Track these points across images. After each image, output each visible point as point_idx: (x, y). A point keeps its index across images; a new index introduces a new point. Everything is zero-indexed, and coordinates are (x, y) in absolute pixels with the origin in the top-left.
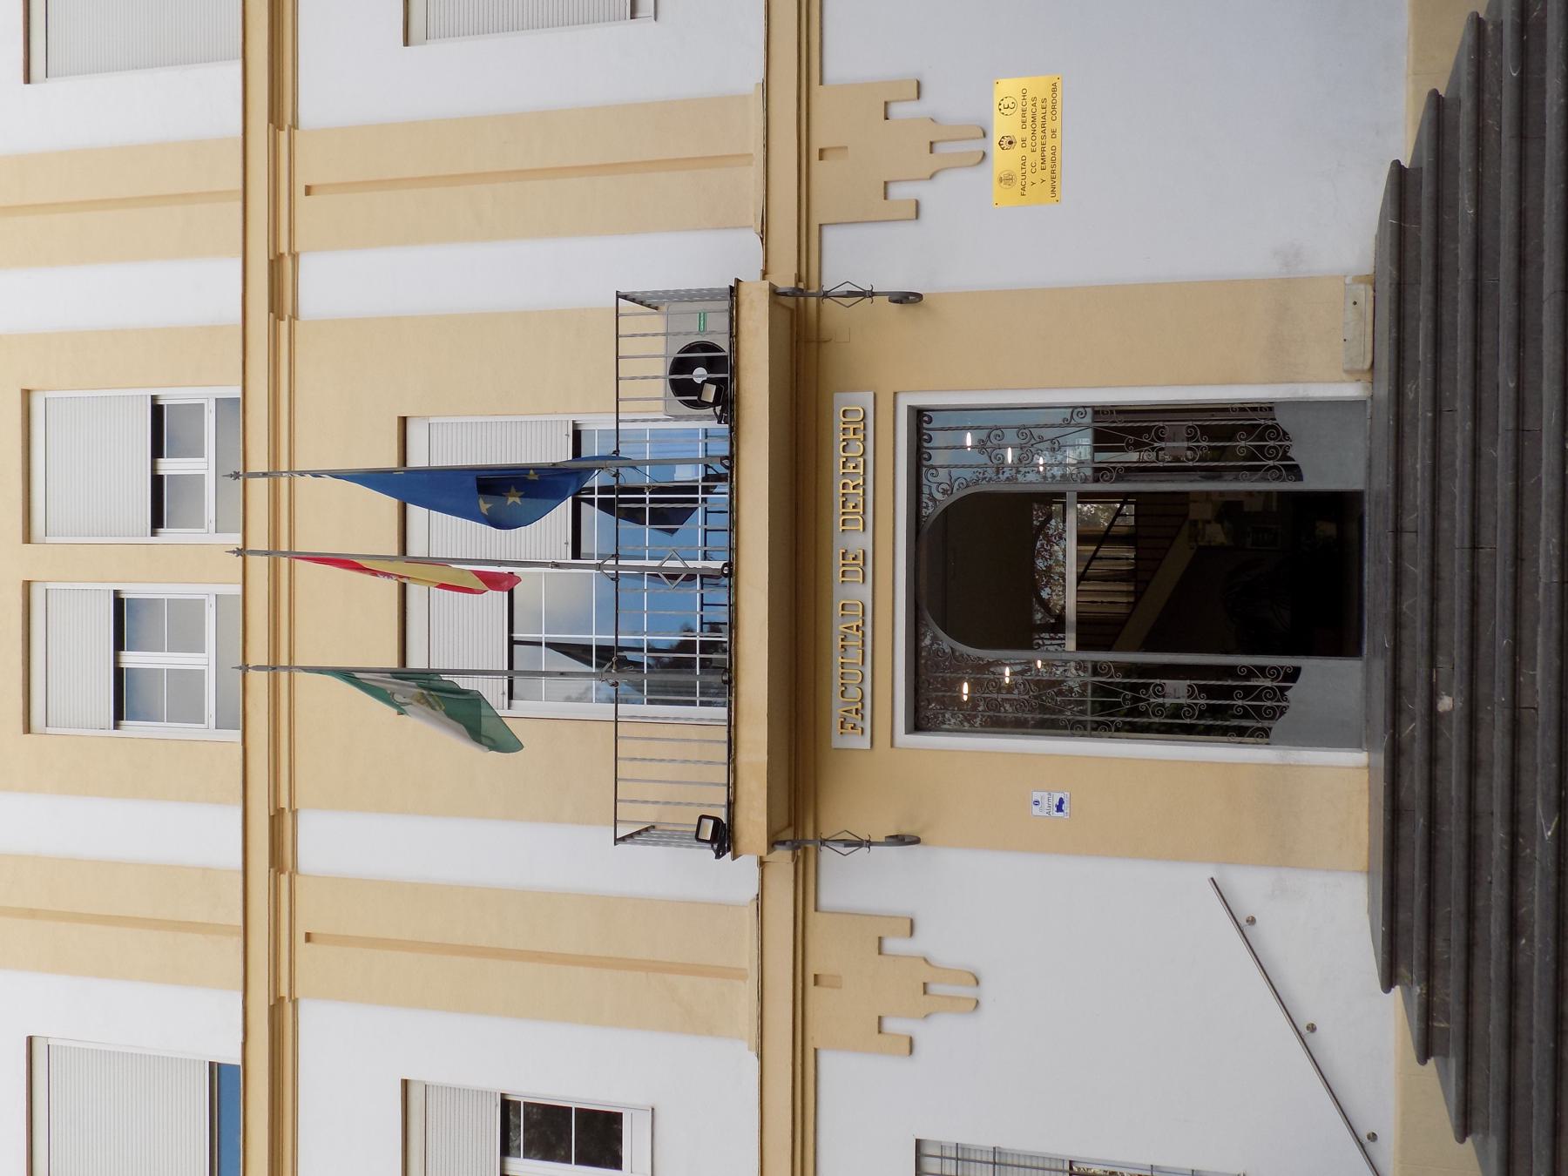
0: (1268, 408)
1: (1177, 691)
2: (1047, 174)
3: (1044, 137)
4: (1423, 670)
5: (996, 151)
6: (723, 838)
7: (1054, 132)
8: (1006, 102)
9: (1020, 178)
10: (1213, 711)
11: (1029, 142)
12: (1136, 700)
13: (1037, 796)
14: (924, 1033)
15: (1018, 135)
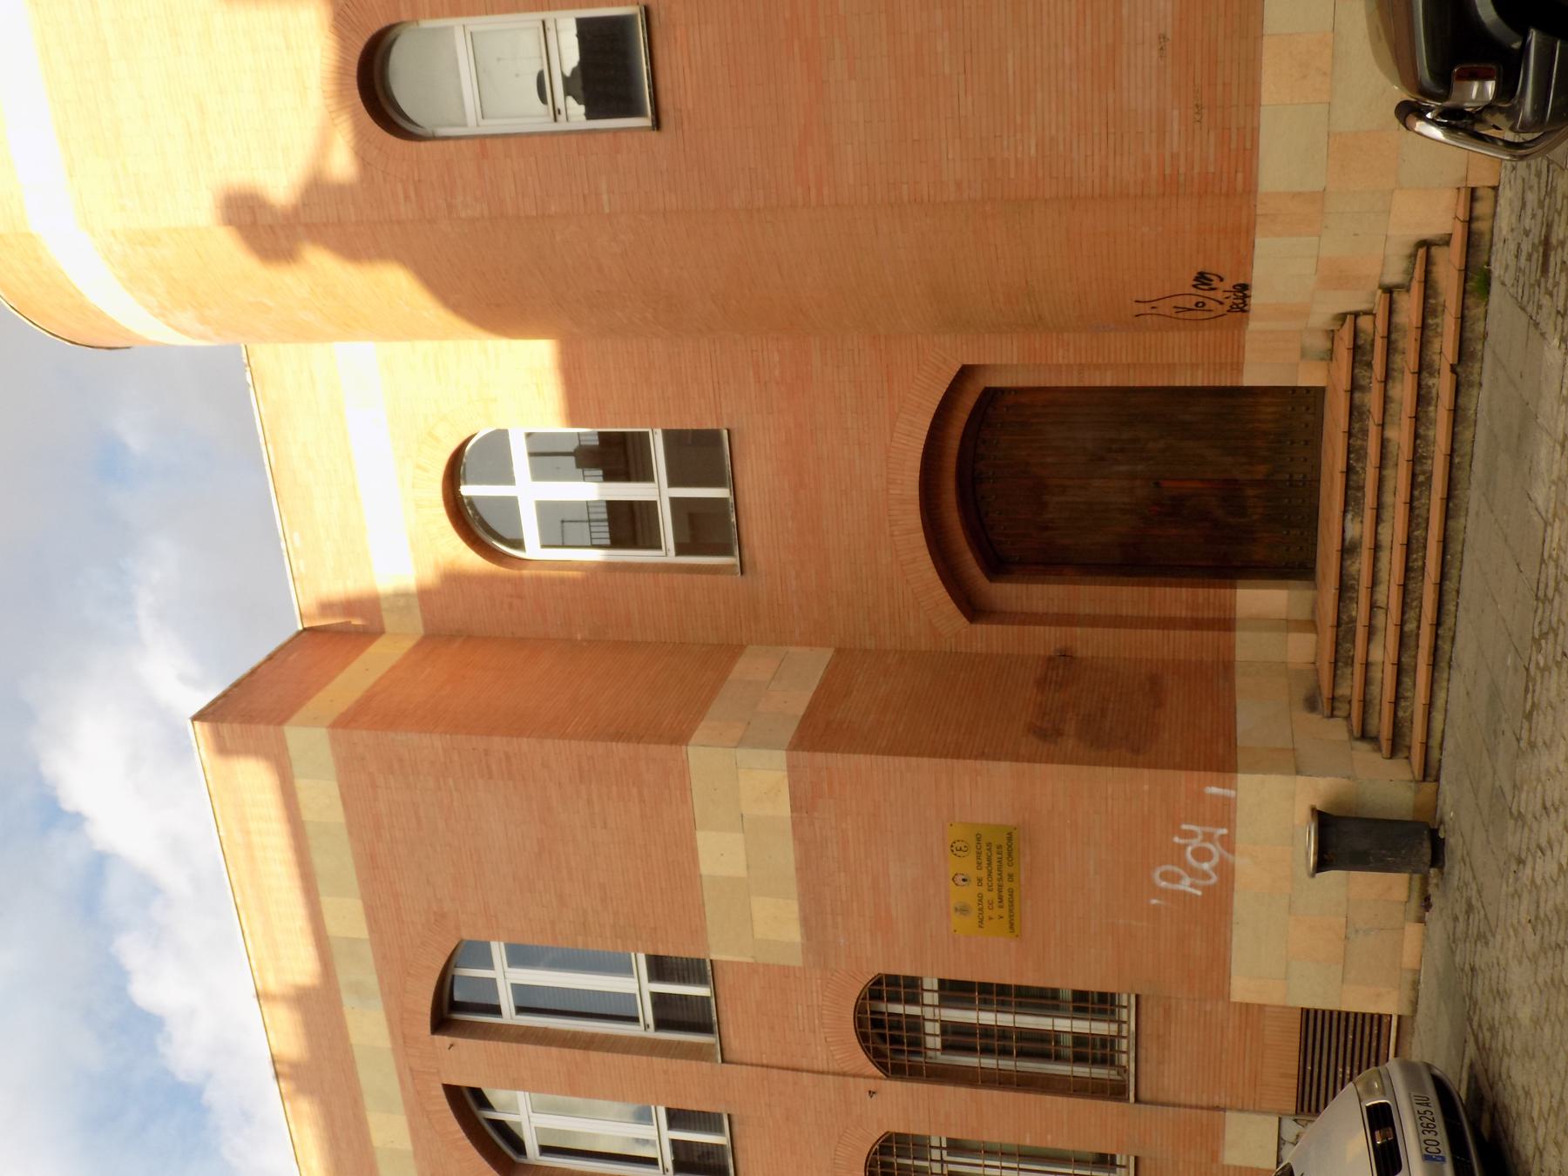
2: (1005, 912)
3: (1000, 879)
7: (1153, 308)
8: (958, 845)
11: (985, 882)
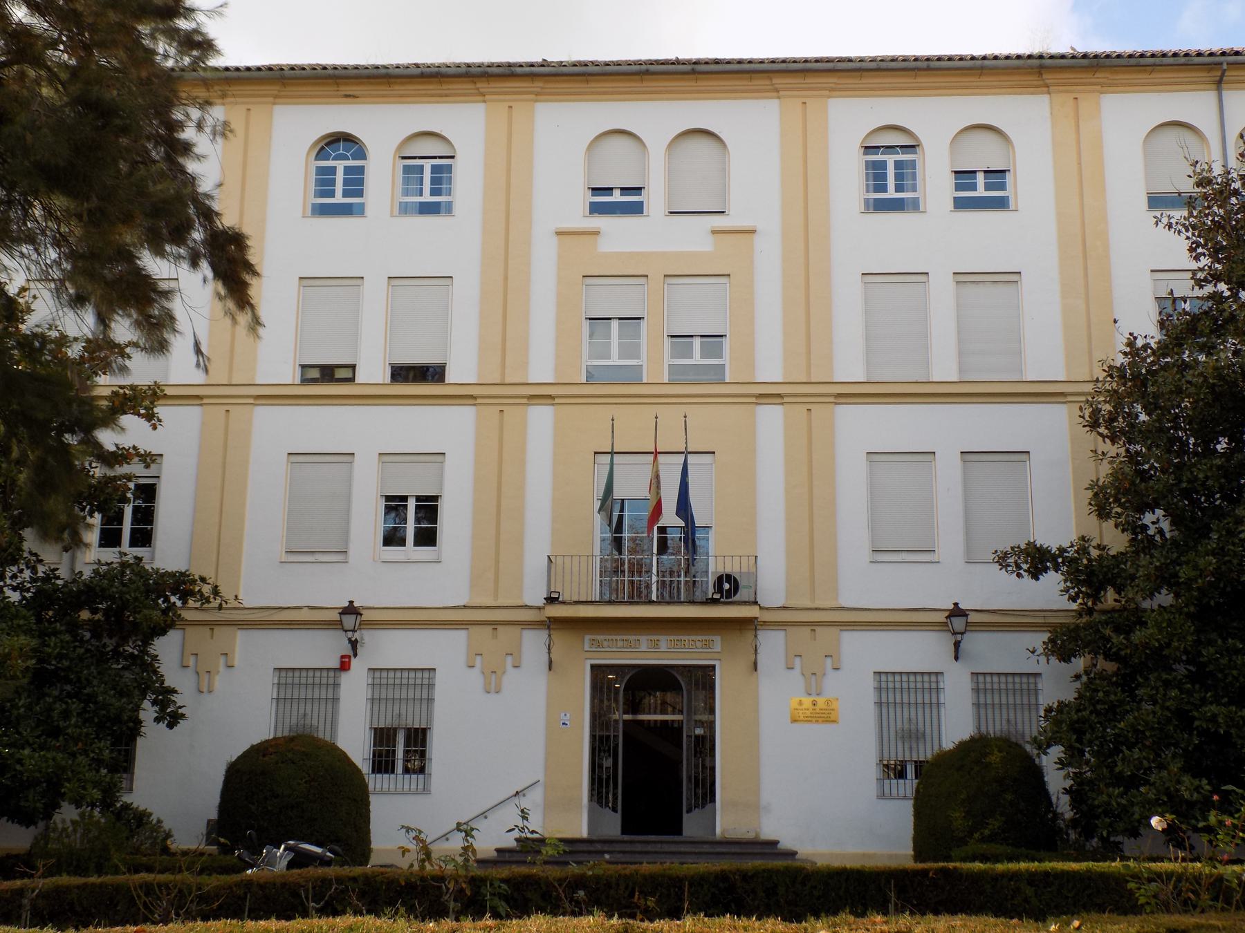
0: (713, 800)
1: (608, 763)
4: (618, 849)
5: (811, 699)
6: (551, 600)
9: (801, 708)
10: (600, 779)
12: (604, 751)
13: (568, 715)
14: (476, 671)
15: (817, 707)
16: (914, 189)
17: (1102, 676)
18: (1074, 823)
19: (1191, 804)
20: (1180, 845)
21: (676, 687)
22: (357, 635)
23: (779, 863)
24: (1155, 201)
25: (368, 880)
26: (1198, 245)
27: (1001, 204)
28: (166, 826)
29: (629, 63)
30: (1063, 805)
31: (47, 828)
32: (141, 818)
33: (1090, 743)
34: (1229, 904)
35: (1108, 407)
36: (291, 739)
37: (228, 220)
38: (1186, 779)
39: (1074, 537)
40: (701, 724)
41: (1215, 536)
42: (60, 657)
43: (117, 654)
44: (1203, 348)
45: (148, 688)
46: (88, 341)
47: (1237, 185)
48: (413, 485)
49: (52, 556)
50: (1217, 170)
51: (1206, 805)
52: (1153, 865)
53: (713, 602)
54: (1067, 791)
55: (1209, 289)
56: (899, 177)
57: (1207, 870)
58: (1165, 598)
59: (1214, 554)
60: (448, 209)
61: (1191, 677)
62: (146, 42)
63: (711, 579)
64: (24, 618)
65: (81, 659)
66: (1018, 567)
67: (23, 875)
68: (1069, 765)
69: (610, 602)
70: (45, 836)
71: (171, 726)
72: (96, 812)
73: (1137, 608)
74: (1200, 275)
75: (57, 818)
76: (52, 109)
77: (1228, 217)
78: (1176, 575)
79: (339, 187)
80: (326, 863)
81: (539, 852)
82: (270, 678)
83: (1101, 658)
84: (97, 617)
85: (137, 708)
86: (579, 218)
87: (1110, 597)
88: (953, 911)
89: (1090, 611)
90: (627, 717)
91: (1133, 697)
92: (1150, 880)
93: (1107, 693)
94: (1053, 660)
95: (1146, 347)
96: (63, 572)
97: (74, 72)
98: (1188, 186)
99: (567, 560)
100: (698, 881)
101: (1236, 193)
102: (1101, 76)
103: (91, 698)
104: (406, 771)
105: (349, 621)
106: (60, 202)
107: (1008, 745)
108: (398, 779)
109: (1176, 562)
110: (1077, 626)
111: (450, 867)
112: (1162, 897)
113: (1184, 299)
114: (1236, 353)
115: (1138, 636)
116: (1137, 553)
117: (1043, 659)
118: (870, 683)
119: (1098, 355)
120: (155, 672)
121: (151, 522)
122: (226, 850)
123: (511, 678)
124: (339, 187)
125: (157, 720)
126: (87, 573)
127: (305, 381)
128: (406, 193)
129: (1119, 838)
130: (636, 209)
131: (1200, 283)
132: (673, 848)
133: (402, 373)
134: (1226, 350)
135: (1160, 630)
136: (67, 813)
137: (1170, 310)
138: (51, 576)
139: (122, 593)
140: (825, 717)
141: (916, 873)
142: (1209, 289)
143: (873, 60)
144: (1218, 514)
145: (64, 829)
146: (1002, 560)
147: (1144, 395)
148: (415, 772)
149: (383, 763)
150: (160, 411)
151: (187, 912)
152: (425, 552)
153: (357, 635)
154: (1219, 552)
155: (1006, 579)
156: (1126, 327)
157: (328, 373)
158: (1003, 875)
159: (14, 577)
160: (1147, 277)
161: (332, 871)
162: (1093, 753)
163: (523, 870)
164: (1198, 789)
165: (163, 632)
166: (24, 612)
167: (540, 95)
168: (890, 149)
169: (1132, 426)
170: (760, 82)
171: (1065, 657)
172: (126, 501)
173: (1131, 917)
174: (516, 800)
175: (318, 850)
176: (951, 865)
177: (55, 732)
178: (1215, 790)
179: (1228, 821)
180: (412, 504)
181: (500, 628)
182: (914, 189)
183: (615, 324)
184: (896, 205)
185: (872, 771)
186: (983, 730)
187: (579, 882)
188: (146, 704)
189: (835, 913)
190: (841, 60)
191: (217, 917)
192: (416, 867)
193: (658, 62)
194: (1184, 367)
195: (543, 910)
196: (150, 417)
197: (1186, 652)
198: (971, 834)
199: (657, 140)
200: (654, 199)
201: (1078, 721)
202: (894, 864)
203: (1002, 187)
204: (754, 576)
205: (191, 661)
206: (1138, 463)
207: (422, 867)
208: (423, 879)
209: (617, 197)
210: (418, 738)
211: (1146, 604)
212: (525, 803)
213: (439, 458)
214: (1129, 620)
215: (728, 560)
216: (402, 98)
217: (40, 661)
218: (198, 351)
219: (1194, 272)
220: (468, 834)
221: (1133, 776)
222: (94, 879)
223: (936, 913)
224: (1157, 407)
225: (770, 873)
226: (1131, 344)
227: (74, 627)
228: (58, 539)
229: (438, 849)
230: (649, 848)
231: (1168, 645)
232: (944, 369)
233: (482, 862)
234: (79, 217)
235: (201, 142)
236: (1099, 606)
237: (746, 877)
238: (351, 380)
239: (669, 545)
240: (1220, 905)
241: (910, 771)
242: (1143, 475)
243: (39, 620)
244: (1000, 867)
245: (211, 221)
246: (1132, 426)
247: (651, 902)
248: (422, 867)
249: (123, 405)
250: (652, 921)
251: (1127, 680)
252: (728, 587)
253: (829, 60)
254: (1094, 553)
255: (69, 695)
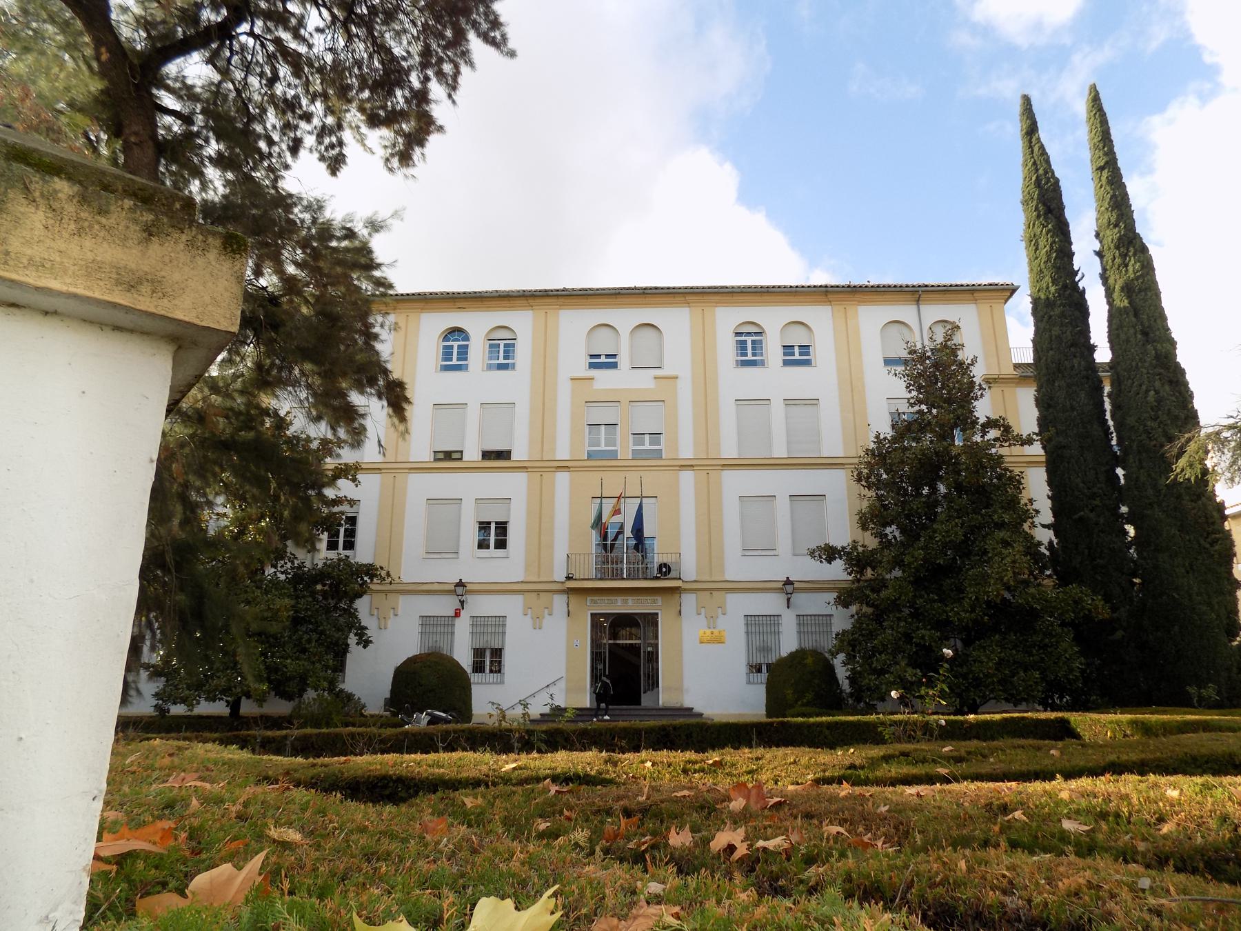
1: (600, 667)
6: (569, 578)
14: (528, 618)
16: (762, 355)
17: (865, 615)
18: (851, 695)
19: (912, 683)
20: (906, 705)
21: (637, 625)
22: (464, 598)
23: (693, 721)
24: (888, 362)
25: (471, 731)
26: (910, 385)
27: (807, 363)
28: (363, 701)
29: (609, 289)
30: (845, 685)
31: (300, 702)
32: (350, 697)
33: (859, 652)
34: (932, 736)
35: (866, 471)
36: (429, 654)
37: (396, 375)
38: (910, 670)
39: (850, 541)
40: (650, 645)
41: (922, 539)
42: (307, 610)
43: (336, 608)
44: (914, 439)
45: (352, 626)
46: (321, 439)
47: (929, 354)
48: (493, 516)
49: (302, 555)
50: (919, 346)
51: (920, 684)
52: (891, 717)
53: (656, 578)
54: (847, 678)
55: (916, 408)
56: (753, 348)
57: (920, 718)
58: (897, 573)
59: (922, 549)
60: (513, 366)
61: (911, 615)
62: (356, 282)
63: (656, 566)
64: (288, 589)
65: (317, 610)
66: (821, 557)
67: (287, 728)
68: (848, 664)
69: (601, 579)
70: (299, 707)
71: (365, 647)
72: (326, 693)
73: (883, 579)
74: (912, 401)
75: (305, 696)
76: (306, 318)
77: (925, 371)
78: (903, 561)
79: (455, 356)
80: (448, 722)
81: (563, 716)
82: (417, 622)
83: (864, 606)
84: (326, 588)
85: (347, 637)
86: (582, 370)
87: (869, 573)
88: (786, 745)
89: (858, 581)
90: (610, 642)
91: (881, 625)
92: (890, 725)
93: (867, 625)
94: (840, 607)
95: (885, 439)
96: (308, 564)
97: (318, 299)
98: (904, 354)
99: (578, 556)
100: (650, 731)
101: (929, 358)
102: (858, 297)
103: (322, 633)
104: (491, 671)
105: (459, 590)
106: (308, 367)
107: (816, 653)
108: (487, 676)
109: (903, 554)
110: (852, 589)
111: (516, 724)
112: (896, 734)
113: (904, 414)
114: (931, 442)
115: (883, 594)
116: (882, 549)
117: (834, 607)
118: (742, 621)
119: (861, 443)
120: (356, 618)
121: (354, 537)
122: (395, 715)
123: (547, 621)
124: (455, 356)
125: (358, 644)
126: (320, 565)
127: (436, 460)
128: (490, 358)
129: (875, 702)
130: (614, 366)
131: (912, 405)
132: (637, 713)
133: (487, 455)
134: (926, 440)
135: (895, 591)
136: (311, 694)
137: (897, 419)
138: (301, 566)
139: (338, 575)
140: (719, 640)
141: (767, 724)
142: (916, 408)
143: (739, 287)
144: (924, 527)
145: (309, 703)
146: (812, 554)
147: (885, 464)
148: (496, 672)
149: (478, 668)
150: (359, 477)
151: (374, 748)
152: (500, 552)
153: (464, 598)
154: (925, 548)
155: (815, 564)
156: (875, 428)
157: (448, 455)
158: (814, 724)
159: (282, 566)
160: (885, 403)
161: (451, 726)
162: (860, 657)
163: (554, 725)
164: (915, 675)
165: (361, 596)
166: (287, 585)
167: (562, 306)
168: (749, 334)
169: (879, 481)
170: (678, 299)
171: (846, 606)
172: (342, 525)
173: (880, 746)
174: (547, 690)
175: (444, 715)
176: (786, 719)
177: (304, 651)
178: (924, 676)
179: (931, 692)
180: (493, 526)
181: (541, 594)
182: (762, 355)
183: (603, 427)
184: (753, 364)
185: (743, 669)
186: (803, 646)
187: (584, 733)
188: (352, 635)
189: (723, 748)
190: (722, 287)
191: (388, 753)
192: (497, 724)
193: (624, 288)
194: (905, 449)
195: (565, 748)
196: (354, 480)
197: (909, 602)
198: (796, 701)
199: (625, 331)
200: (624, 361)
201: (853, 640)
202: (755, 720)
203: (808, 354)
204: (679, 563)
205: (375, 612)
206: (883, 501)
207: (500, 724)
208: (501, 731)
209: (603, 359)
210: (497, 653)
211: (888, 577)
212: (552, 690)
213: (508, 501)
214: (878, 585)
215: (669, 555)
216: (488, 308)
217: (296, 612)
218: (380, 445)
219: (909, 399)
220: (526, 706)
221: (882, 669)
222: (324, 730)
223: (778, 746)
224: (892, 471)
225: (689, 726)
226: (877, 437)
227: (313, 594)
228: (304, 546)
229: (509, 714)
230: (624, 712)
231: (899, 598)
232: (780, 451)
233: (533, 721)
234: (319, 374)
235: (384, 334)
236: (863, 578)
237: (675, 728)
238: (461, 459)
239: (1069, 782)
240: (927, 737)
241: (764, 668)
242: (884, 506)
243: (296, 590)
244: (811, 720)
245: (387, 376)
246: (879, 481)
247: (624, 743)
248: (500, 724)
249: (340, 473)
250: (624, 753)
251: (879, 617)
252: (665, 570)
253: (716, 288)
254: (860, 549)
255: (312, 631)
